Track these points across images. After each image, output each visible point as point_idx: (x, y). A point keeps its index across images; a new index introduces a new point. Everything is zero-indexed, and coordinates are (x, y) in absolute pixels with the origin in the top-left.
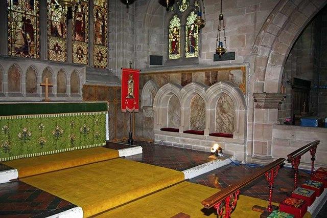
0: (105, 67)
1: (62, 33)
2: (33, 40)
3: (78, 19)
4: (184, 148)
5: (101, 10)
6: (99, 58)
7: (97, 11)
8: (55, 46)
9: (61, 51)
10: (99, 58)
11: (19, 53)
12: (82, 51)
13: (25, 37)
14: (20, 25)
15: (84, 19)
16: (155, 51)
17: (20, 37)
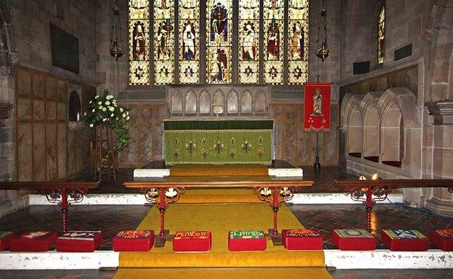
0: (279, 84)
1: (254, 56)
2: (226, 67)
3: (272, 38)
4: (15, 143)
5: (299, 23)
6: (297, 74)
7: (295, 24)
8: (246, 69)
9: (253, 73)
10: (297, 74)
11: (214, 80)
12: (275, 70)
13: (219, 65)
14: (216, 56)
15: (278, 37)
16: (361, 57)
17: (215, 66)
